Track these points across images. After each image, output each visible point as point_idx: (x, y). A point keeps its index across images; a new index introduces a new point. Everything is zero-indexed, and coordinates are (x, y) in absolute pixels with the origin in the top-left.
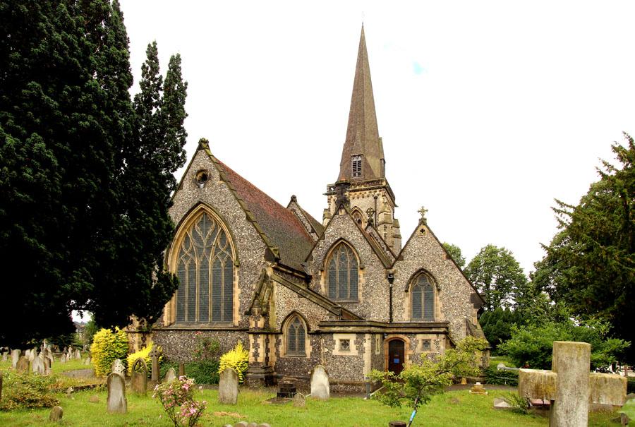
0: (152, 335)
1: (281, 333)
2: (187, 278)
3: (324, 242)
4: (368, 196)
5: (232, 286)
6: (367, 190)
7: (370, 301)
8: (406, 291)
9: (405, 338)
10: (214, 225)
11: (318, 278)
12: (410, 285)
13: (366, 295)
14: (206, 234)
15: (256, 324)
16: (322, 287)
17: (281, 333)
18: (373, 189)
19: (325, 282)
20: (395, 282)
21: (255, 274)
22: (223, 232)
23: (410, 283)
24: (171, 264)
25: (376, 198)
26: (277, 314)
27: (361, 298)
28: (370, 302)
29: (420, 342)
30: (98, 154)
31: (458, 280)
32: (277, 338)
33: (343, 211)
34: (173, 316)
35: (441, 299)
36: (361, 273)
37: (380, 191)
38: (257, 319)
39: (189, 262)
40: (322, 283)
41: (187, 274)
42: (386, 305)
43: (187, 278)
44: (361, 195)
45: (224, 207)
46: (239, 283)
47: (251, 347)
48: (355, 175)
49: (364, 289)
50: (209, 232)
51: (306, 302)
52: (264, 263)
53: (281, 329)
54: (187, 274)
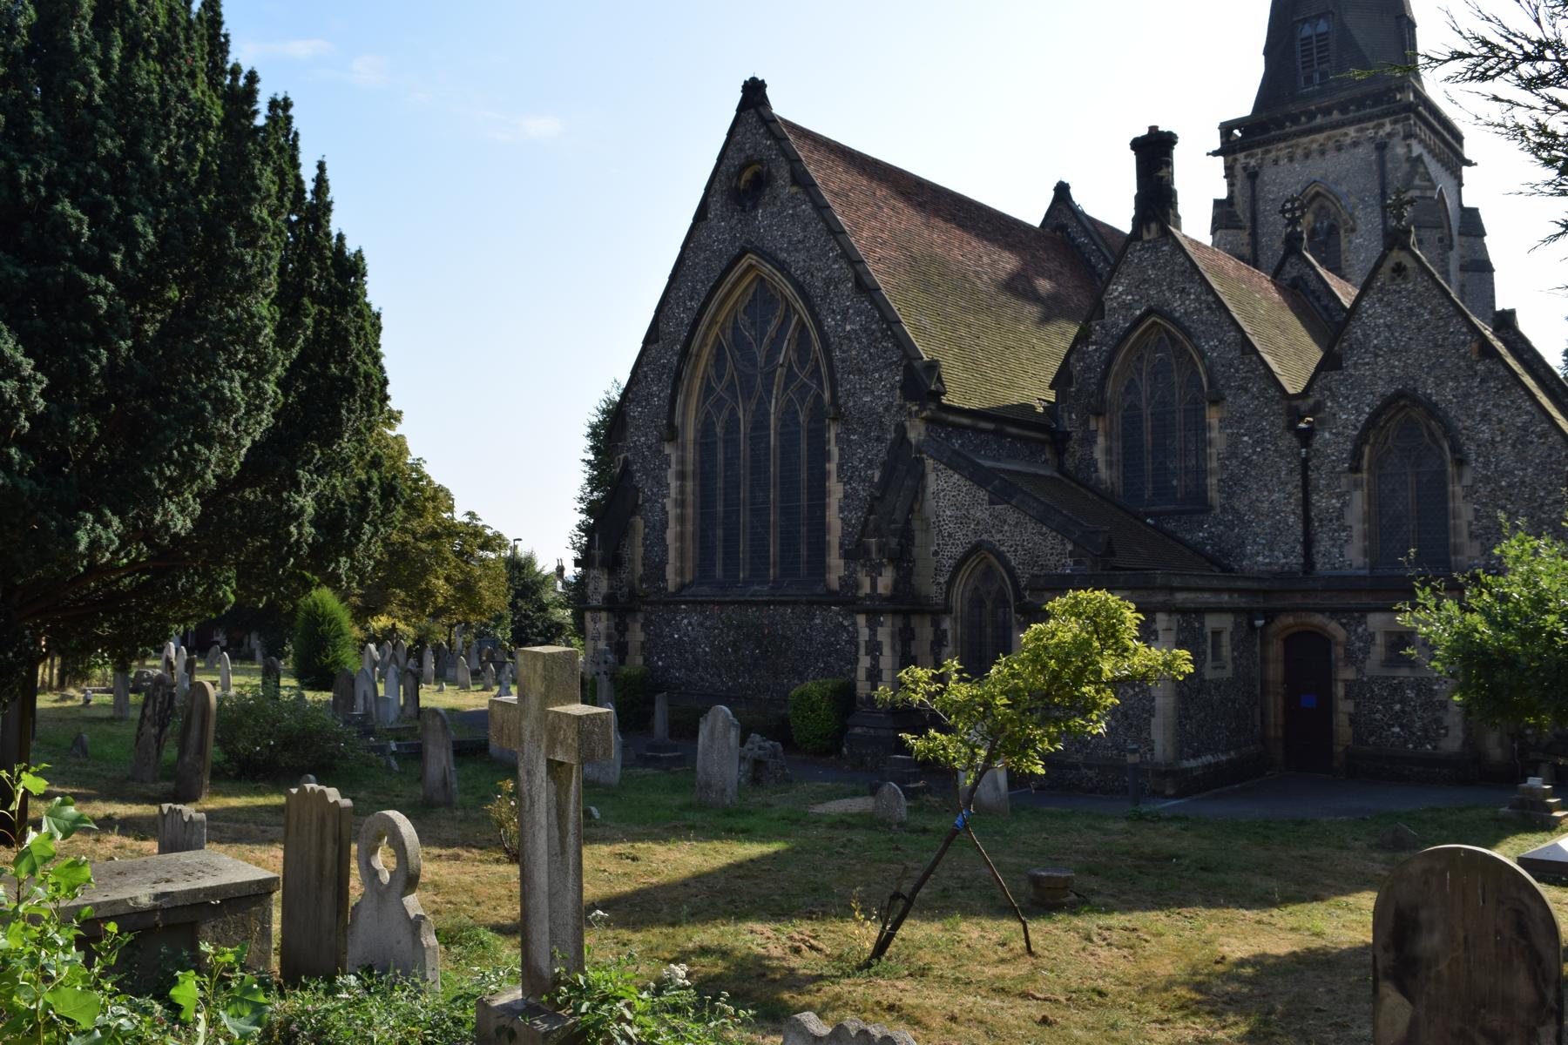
0: (640, 617)
1: (947, 610)
2: (720, 457)
3: (1103, 327)
4: (1355, 144)
5: (824, 476)
6: (1351, 123)
7: (1241, 504)
8: (1355, 469)
9: (1334, 628)
10: (782, 307)
11: (1089, 440)
12: (1367, 450)
13: (1232, 485)
14: (763, 334)
15: (874, 586)
16: (1101, 465)
17: (947, 610)
18: (1370, 118)
19: (1108, 451)
20: (1317, 442)
21: (878, 439)
22: (802, 326)
23: (1366, 442)
24: (683, 424)
25: (1381, 147)
26: (936, 553)
27: (1215, 496)
28: (1243, 509)
29: (1379, 639)
30: (197, 240)
31: (1525, 428)
32: (936, 625)
33: (1154, 226)
34: (689, 565)
35: (1470, 492)
36: (1213, 416)
37: (1395, 122)
38: (875, 571)
39: (725, 413)
40: (1099, 453)
41: (720, 445)
42: (1291, 520)
43: (720, 457)
44: (1331, 144)
45: (802, 256)
46: (840, 467)
47: (862, 651)
48: (1309, 80)
49: (1224, 467)
50: (771, 330)
51: (1012, 517)
52: (902, 407)
53: (947, 599)
54: (720, 445)
